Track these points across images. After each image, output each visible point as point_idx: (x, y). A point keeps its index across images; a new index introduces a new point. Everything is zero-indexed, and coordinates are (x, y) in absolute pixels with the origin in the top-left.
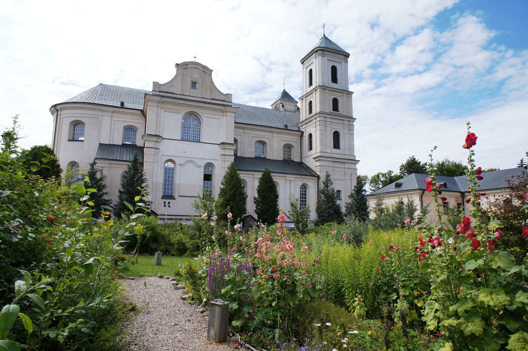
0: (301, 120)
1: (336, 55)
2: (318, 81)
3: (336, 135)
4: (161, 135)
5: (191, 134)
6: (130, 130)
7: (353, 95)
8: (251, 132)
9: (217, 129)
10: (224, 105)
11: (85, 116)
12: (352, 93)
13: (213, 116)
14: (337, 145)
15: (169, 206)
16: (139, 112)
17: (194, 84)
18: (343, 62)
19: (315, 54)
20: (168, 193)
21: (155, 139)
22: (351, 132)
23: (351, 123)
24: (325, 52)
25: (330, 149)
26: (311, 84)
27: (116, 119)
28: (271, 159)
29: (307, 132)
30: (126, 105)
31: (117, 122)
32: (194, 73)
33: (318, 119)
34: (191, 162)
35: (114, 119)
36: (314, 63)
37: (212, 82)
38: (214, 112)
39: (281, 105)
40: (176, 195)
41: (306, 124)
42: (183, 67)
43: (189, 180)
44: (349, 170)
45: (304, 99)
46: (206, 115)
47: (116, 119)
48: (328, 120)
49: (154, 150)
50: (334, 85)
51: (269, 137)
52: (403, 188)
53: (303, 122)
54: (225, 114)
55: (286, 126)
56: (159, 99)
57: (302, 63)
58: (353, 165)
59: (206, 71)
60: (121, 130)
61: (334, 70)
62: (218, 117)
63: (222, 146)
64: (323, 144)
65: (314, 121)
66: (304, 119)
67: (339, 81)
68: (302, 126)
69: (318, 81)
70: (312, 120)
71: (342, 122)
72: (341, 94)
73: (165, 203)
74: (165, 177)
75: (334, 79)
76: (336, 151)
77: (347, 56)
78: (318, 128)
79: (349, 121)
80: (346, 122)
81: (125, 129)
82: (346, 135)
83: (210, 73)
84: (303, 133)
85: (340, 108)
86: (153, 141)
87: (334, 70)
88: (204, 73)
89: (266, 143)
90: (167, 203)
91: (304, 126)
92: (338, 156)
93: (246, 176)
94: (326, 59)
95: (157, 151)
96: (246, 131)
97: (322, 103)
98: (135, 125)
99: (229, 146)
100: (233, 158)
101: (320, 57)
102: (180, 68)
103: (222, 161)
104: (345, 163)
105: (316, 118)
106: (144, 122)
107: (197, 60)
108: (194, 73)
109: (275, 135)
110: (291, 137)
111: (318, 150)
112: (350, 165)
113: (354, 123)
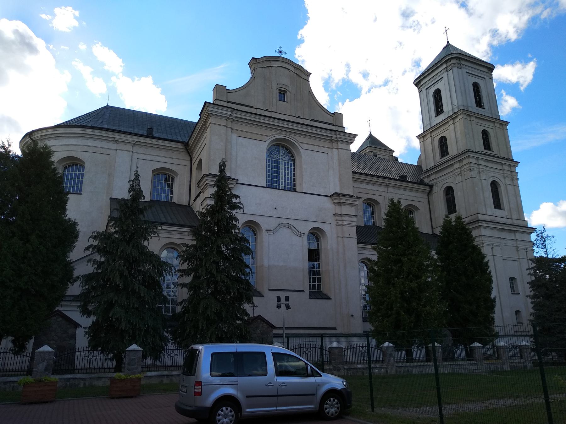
3: (494, 186)
11: (85, 149)
12: (507, 123)
13: (316, 148)
15: (288, 307)
16: (180, 146)
17: (282, 94)
19: (444, 66)
27: (141, 156)
31: (141, 162)
34: (287, 226)
35: (136, 156)
36: (445, 78)
38: (317, 142)
44: (522, 243)
46: (305, 146)
47: (141, 156)
48: (481, 162)
50: (480, 111)
51: (383, 194)
53: (427, 171)
54: (335, 145)
58: (526, 236)
61: (476, 86)
62: (324, 150)
63: (336, 198)
67: (486, 106)
68: (429, 176)
69: (455, 103)
70: (452, 165)
71: (500, 167)
72: (492, 124)
73: (279, 299)
75: (479, 104)
76: (498, 212)
79: (510, 166)
80: (506, 167)
81: (155, 175)
82: (510, 188)
83: (306, 78)
87: (476, 86)
88: (298, 78)
89: (377, 203)
90: (283, 300)
91: (432, 177)
92: (503, 220)
94: (465, 71)
98: (174, 168)
101: (455, 69)
102: (260, 66)
103: (337, 224)
104: (514, 231)
106: (189, 159)
110: (410, 193)
112: (522, 235)
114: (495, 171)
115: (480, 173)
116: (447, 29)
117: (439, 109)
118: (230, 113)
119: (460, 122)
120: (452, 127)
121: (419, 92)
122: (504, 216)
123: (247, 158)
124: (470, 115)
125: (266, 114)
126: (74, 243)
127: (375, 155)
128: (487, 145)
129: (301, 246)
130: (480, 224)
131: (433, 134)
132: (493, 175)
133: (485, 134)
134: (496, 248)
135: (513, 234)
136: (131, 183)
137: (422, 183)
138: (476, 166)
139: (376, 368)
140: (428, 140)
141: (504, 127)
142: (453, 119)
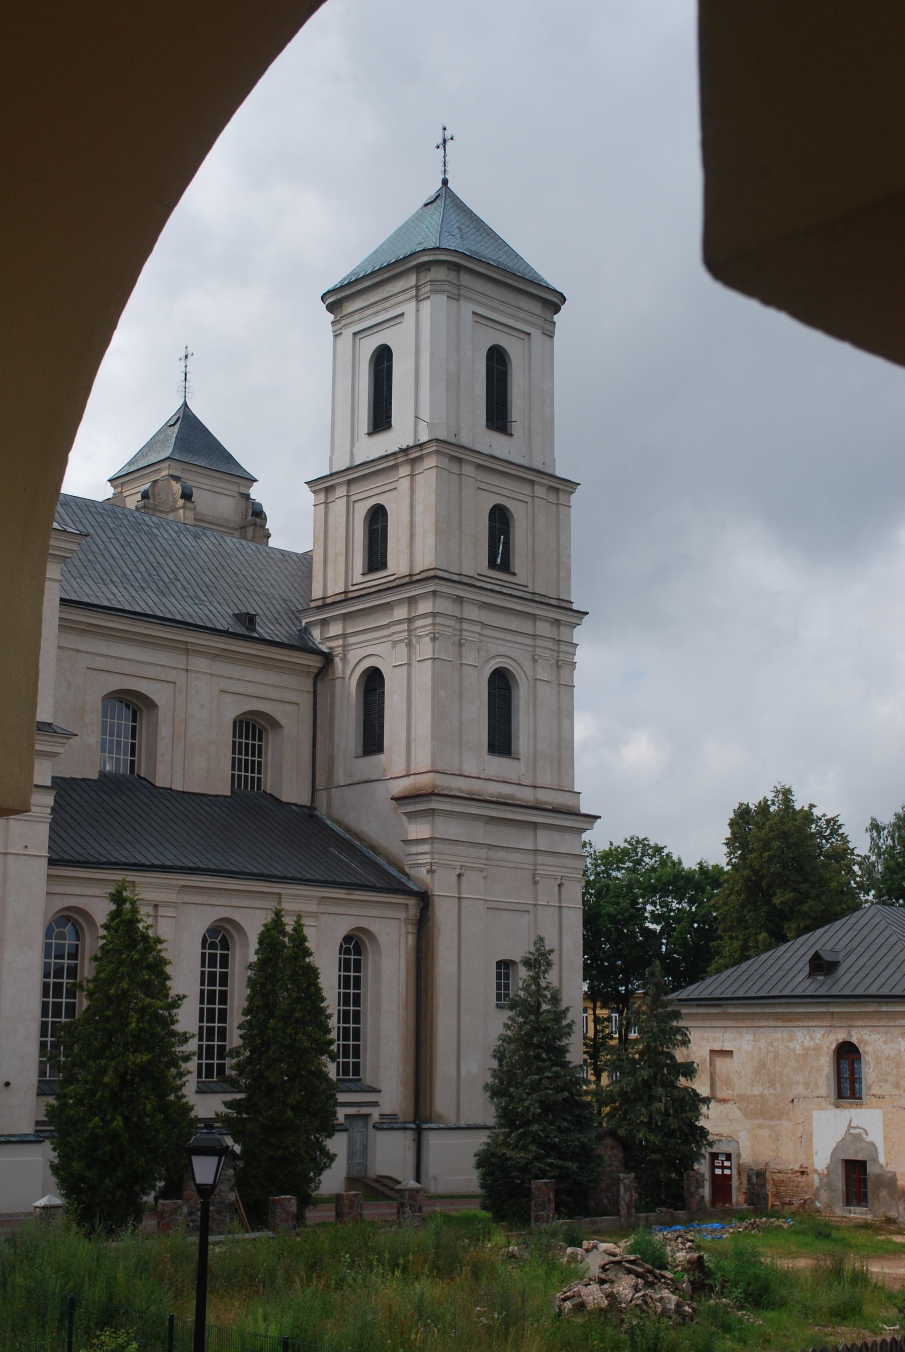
0: (317, 593)
1: (511, 297)
2: (425, 414)
3: (501, 685)
14: (501, 741)
18: (536, 334)
19: (412, 280)
22: (564, 672)
23: (564, 632)
24: (466, 280)
25: (480, 767)
26: (381, 419)
28: (178, 787)
29: (353, 656)
33: (425, 607)
39: (177, 488)
41: (345, 617)
45: (341, 491)
48: (472, 612)
51: (171, 675)
52: (845, 981)
53: (325, 606)
55: (249, 620)
57: (331, 308)
58: (569, 837)
61: (497, 362)
64: (444, 732)
65: (401, 613)
66: (336, 587)
67: (517, 428)
68: (324, 623)
69: (425, 414)
70: (388, 606)
72: (526, 489)
75: (498, 417)
76: (498, 765)
77: (552, 302)
78: (425, 649)
79: (557, 623)
80: (543, 629)
82: (543, 691)
84: (328, 658)
85: (519, 561)
87: (497, 362)
89: (150, 704)
91: (335, 629)
93: (374, 912)
94: (467, 308)
97: (447, 527)
101: (443, 297)
104: (535, 826)
109: (200, 663)
110: (271, 677)
111: (423, 760)
112: (556, 836)
113: (579, 635)
114: (510, 637)
115: (461, 645)
116: (448, 134)
117: (381, 419)
119: (428, 477)
120: (404, 484)
121: (336, 336)
122: (514, 778)
124: (460, 460)
127: (187, 496)
128: (500, 555)
130: (433, 805)
131: (356, 489)
132: (501, 650)
133: (500, 520)
134: (469, 876)
135: (530, 833)
137: (303, 645)
138: (452, 623)
139: (217, 1243)
140: (339, 507)
141: (562, 498)
142: (413, 462)
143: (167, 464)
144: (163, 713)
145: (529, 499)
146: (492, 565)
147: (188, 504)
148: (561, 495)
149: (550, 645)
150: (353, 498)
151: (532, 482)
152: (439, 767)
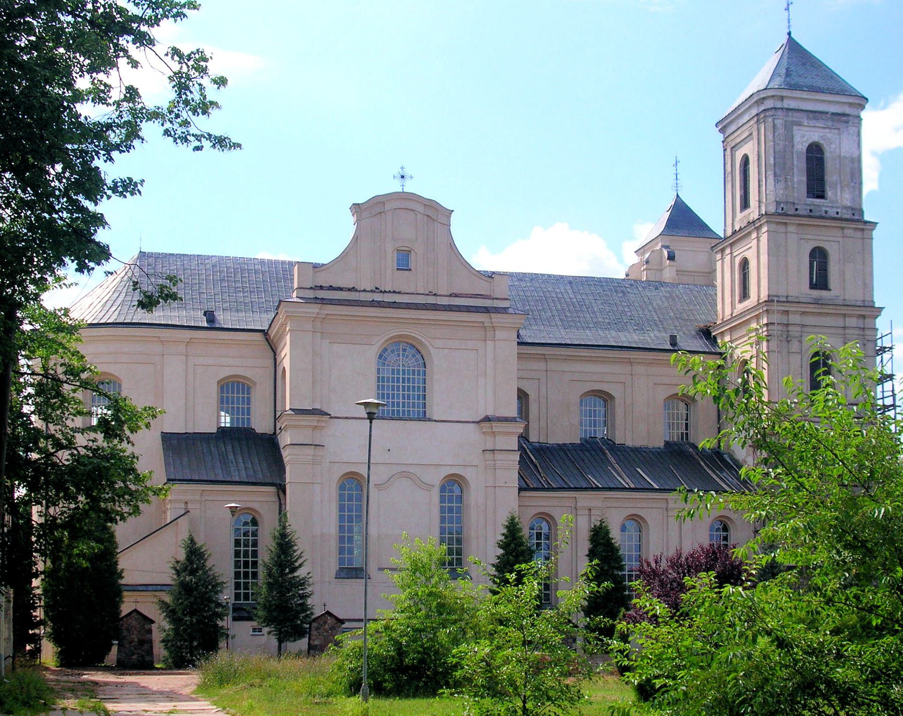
4: (325, 409)
5: (402, 398)
6: (233, 391)
7: (874, 233)
8: (566, 366)
9: (473, 379)
10: (486, 310)
16: (258, 337)
17: (404, 263)
20: (350, 561)
21: (313, 420)
30: (222, 319)
32: (403, 224)
37: (452, 246)
40: (372, 569)
41: (731, 330)
42: (369, 213)
43: (405, 530)
45: (728, 251)
46: (439, 343)
49: (310, 451)
53: (725, 323)
56: (314, 309)
57: (722, 131)
59: (435, 215)
60: (214, 389)
65: (754, 325)
70: (747, 322)
71: (840, 322)
74: (341, 518)
80: (852, 322)
83: (443, 220)
86: (305, 426)
89: (611, 397)
91: (727, 338)
95: (319, 452)
96: (552, 365)
98: (248, 373)
99: (504, 424)
100: (517, 457)
105: (757, 317)
107: (410, 187)
108: (403, 224)
109: (640, 369)
118: (317, 311)
123: (351, 372)
125: (378, 297)
126: (399, 695)
128: (820, 281)
129: (428, 507)
131: (735, 248)
133: (819, 256)
136: (178, 141)
143: (660, 238)
144: (618, 402)
145: (840, 239)
146: (813, 286)
147: (673, 263)
148: (866, 232)
149: (856, 332)
150: (735, 254)
151: (785, 224)
152: (172, 477)
